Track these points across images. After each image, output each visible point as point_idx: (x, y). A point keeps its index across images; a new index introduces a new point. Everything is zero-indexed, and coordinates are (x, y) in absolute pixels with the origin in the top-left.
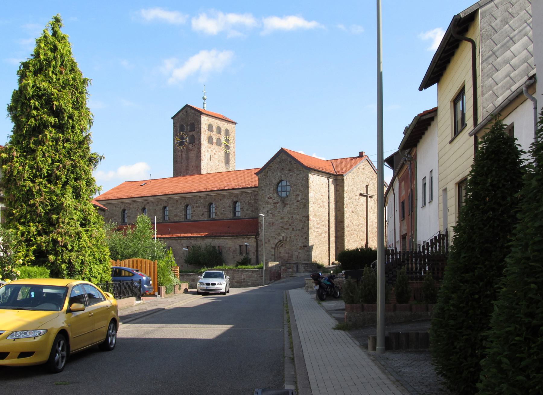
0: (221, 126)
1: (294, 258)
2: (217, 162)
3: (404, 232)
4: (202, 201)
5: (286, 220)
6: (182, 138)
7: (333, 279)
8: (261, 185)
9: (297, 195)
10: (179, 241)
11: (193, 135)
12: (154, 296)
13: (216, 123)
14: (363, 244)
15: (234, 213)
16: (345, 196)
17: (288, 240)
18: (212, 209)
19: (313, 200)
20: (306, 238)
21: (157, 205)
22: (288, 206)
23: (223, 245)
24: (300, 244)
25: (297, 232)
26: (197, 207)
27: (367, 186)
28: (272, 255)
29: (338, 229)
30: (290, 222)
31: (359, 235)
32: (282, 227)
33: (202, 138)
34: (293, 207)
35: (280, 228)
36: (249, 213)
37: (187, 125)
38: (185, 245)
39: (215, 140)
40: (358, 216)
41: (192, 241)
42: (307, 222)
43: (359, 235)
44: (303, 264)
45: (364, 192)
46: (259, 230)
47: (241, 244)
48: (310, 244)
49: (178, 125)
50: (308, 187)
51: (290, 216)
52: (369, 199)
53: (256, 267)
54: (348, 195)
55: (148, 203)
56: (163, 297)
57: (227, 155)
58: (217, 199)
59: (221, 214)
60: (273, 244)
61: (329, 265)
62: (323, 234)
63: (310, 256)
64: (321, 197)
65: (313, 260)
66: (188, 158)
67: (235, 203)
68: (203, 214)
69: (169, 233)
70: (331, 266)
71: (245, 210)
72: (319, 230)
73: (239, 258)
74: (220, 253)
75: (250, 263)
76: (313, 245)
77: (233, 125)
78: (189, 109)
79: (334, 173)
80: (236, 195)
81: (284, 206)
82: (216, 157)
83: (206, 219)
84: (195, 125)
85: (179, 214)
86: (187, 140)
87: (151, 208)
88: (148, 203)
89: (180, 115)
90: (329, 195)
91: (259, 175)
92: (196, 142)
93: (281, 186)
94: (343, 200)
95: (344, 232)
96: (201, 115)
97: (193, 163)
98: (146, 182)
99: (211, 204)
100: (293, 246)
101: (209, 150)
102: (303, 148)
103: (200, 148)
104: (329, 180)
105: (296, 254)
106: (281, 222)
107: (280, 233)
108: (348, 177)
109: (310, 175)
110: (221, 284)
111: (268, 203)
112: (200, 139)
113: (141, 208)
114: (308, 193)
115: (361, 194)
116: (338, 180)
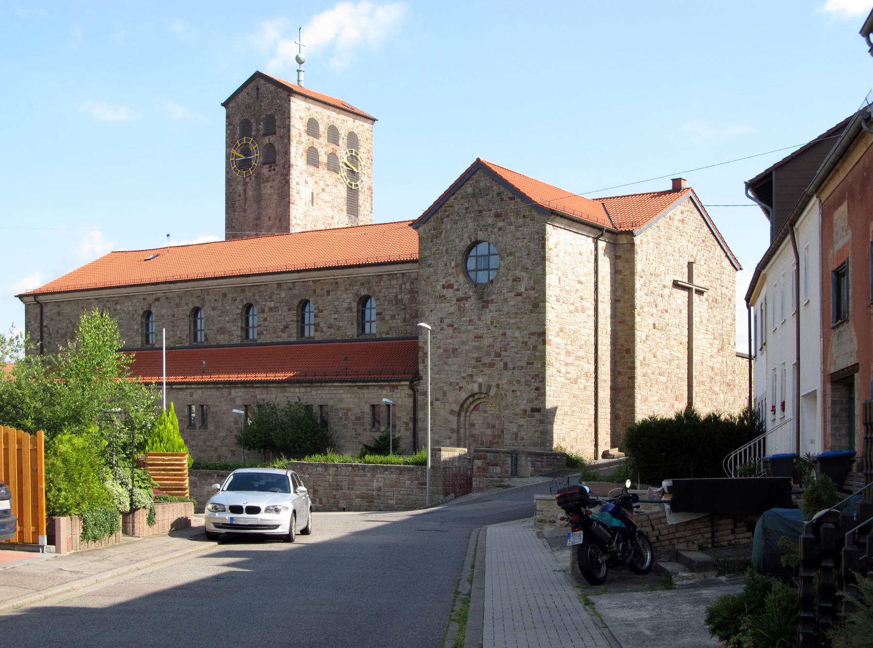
0: (338, 124)
1: (508, 439)
2: (329, 210)
3: (842, 362)
4: (283, 294)
5: (486, 341)
6: (246, 152)
7: (631, 509)
8: (427, 254)
9: (516, 280)
10: (225, 391)
11: (271, 146)
12: (35, 547)
13: (326, 117)
14: (681, 406)
15: (361, 325)
16: (638, 285)
17: (492, 393)
18: (307, 315)
19: (558, 292)
20: (537, 389)
21: (178, 306)
22: (492, 307)
23: (331, 403)
25: (516, 372)
26: (271, 309)
27: (690, 265)
28: (452, 431)
29: (619, 369)
30: (497, 346)
31: (670, 386)
32: (478, 360)
34: (505, 309)
35: (473, 362)
36: (397, 325)
37: (258, 118)
38: (239, 402)
39: (323, 159)
40: (668, 339)
41: (257, 391)
42: (540, 347)
43: (670, 386)
44: (531, 454)
45: (683, 279)
46: (421, 367)
47: (375, 402)
48: (549, 405)
49: (237, 121)
50: (544, 258)
51: (497, 332)
52: (695, 297)
53: (409, 459)
55: (157, 300)
56: (64, 552)
57: (353, 195)
58: (318, 291)
59: (330, 327)
60: (455, 402)
61: (596, 458)
62: (582, 381)
63: (547, 435)
64: (578, 286)
65: (555, 446)
66: (259, 199)
67: (363, 301)
68: (286, 327)
69: (204, 373)
70: (601, 460)
71: (388, 318)
72: (570, 369)
73: (370, 436)
74: (325, 423)
75: (397, 450)
76: (555, 409)
77: (367, 125)
78: (262, 81)
79: (608, 225)
81: (483, 307)
82: (325, 196)
84: (275, 121)
85: (229, 325)
86: (257, 156)
87: (163, 311)
88: (157, 300)
89: (241, 96)
90: (596, 283)
91: (421, 229)
92: (277, 160)
93: (477, 256)
94: (633, 297)
95: (633, 378)
96: (289, 96)
97: (271, 211)
98: (157, 253)
99: (305, 303)
100: (506, 407)
102: (534, 164)
104: (596, 244)
105: (513, 428)
106: (477, 348)
107: (471, 376)
108: (645, 239)
109: (549, 228)
110: (277, 511)
111: (442, 297)
112: (287, 153)
113: (141, 312)
114: (544, 274)
115: (676, 284)
116: (620, 244)
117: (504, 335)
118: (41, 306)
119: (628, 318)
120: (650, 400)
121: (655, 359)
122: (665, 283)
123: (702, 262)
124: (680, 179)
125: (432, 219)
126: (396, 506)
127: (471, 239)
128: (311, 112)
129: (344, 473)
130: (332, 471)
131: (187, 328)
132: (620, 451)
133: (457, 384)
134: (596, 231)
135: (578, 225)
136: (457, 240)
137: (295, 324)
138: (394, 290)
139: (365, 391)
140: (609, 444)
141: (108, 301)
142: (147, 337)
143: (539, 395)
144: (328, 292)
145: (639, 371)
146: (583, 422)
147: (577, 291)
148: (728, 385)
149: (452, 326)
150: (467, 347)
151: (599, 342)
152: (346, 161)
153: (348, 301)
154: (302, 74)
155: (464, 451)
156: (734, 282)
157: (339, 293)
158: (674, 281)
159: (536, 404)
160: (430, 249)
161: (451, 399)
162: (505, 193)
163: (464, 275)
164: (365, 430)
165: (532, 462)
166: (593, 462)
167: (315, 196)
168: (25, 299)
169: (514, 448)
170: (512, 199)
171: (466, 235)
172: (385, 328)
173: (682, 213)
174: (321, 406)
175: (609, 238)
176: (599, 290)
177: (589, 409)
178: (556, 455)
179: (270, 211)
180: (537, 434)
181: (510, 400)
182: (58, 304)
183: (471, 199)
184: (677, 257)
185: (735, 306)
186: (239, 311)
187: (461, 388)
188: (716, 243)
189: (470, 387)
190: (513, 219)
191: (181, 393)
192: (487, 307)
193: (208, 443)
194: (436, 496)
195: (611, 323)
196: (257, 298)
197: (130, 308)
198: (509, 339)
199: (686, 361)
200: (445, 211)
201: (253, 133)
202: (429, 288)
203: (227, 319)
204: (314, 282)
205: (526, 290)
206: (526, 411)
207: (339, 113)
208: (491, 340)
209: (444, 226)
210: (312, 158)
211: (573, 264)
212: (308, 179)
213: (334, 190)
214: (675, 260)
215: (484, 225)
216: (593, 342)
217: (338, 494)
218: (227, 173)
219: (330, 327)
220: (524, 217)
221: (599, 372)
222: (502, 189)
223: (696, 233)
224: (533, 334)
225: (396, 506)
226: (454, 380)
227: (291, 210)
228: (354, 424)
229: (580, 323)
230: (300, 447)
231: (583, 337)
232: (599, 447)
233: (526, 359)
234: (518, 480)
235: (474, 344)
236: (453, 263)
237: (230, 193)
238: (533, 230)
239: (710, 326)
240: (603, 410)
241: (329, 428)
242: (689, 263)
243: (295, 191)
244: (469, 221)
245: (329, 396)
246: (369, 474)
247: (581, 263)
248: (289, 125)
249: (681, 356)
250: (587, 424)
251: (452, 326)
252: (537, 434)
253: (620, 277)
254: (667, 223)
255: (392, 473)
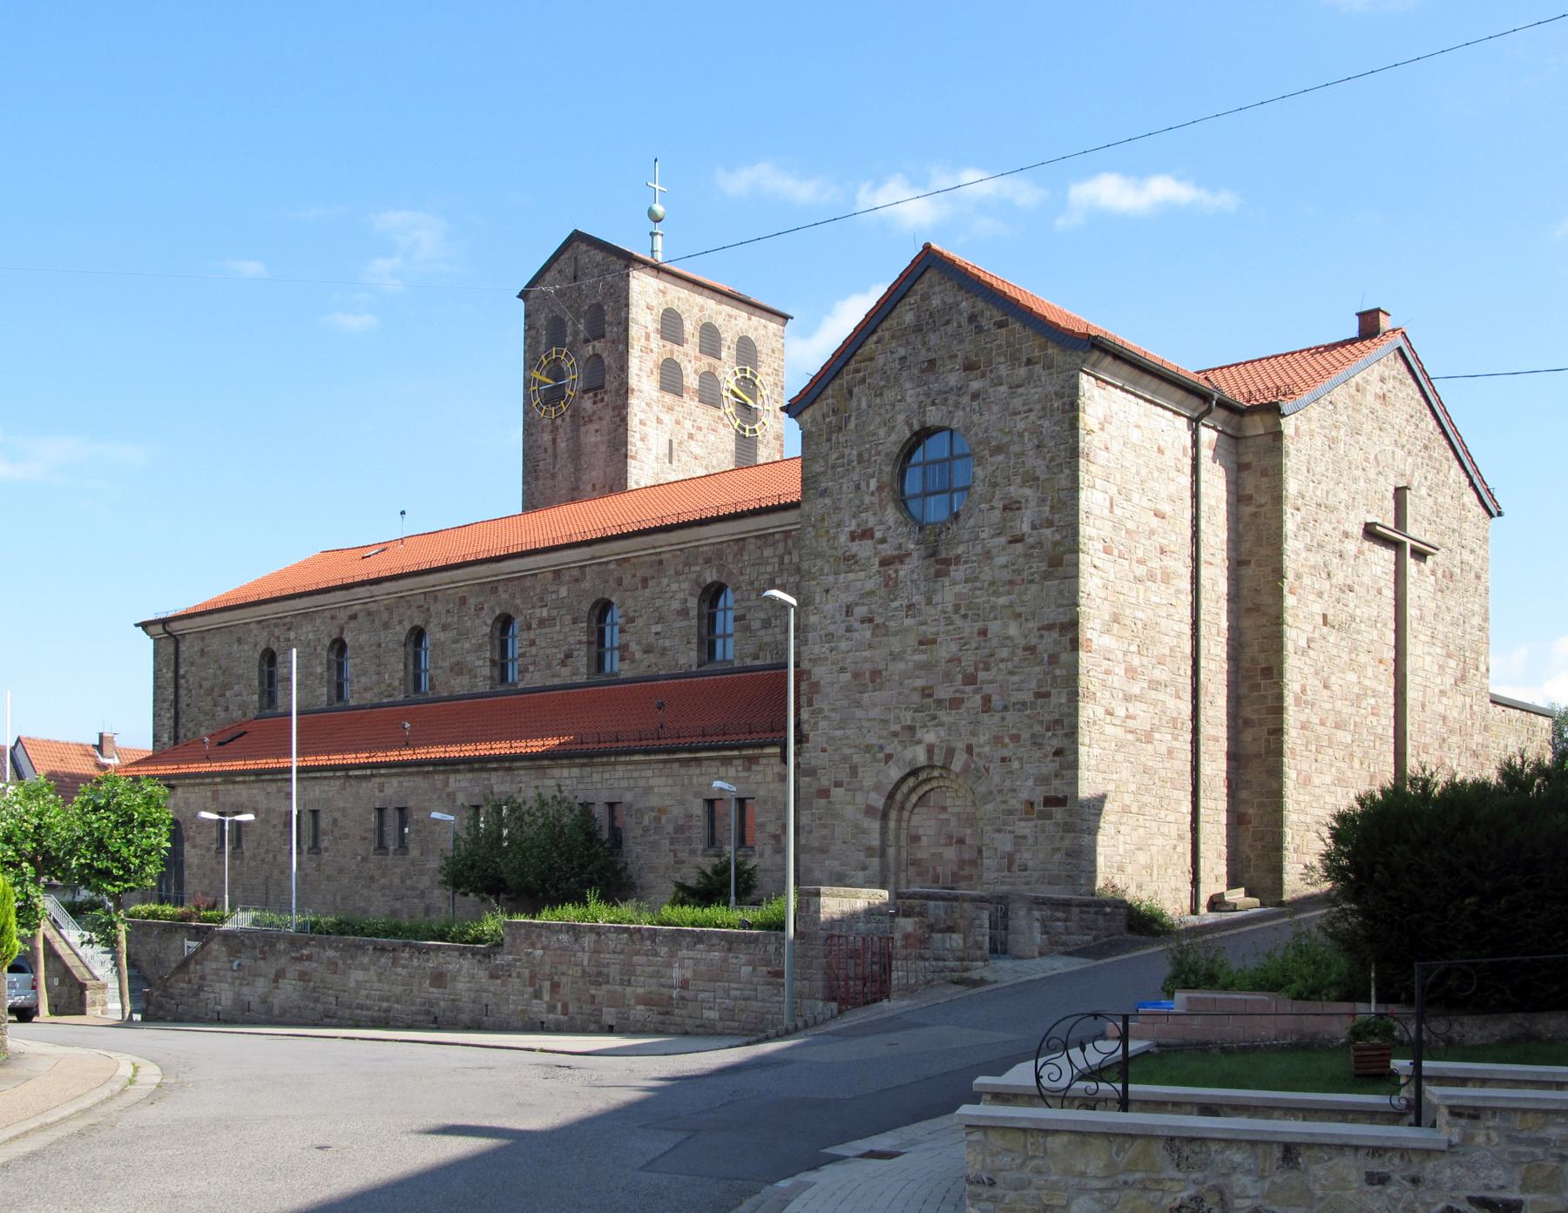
0: (719, 321)
4: (563, 592)
5: (945, 650)
6: (557, 373)
8: (817, 468)
9: (1012, 507)
11: (597, 357)
13: (696, 309)
15: (708, 645)
16: (1290, 526)
17: (957, 765)
19: (1107, 530)
20: (1058, 753)
22: (959, 572)
23: (628, 797)
24: (1030, 790)
25: (1011, 716)
26: (542, 623)
27: (1400, 494)
28: (870, 851)
29: (1248, 712)
30: (968, 660)
31: (1358, 752)
32: (926, 692)
33: (634, 363)
34: (987, 575)
35: (916, 697)
37: (576, 316)
39: (691, 381)
40: (1354, 649)
41: (494, 778)
42: (1064, 657)
43: (1358, 752)
44: (1039, 902)
48: (1086, 790)
49: (542, 321)
50: (1074, 453)
51: (969, 628)
54: (1303, 526)
55: (353, 617)
58: (627, 580)
59: (648, 650)
60: (877, 788)
62: (1164, 737)
63: (1082, 859)
65: (1100, 883)
66: (576, 454)
68: (568, 656)
70: (1207, 917)
71: (756, 625)
72: (1137, 708)
73: (697, 865)
76: (1101, 799)
77: (774, 326)
78: (584, 247)
80: (715, 556)
81: (938, 574)
82: (694, 447)
83: (582, 678)
84: (603, 314)
86: (574, 380)
87: (363, 638)
88: (353, 617)
91: (806, 415)
92: (607, 385)
95: (1278, 731)
96: (627, 267)
100: (988, 797)
101: (666, 417)
103: (625, 406)
105: (1004, 843)
106: (923, 666)
107: (911, 729)
108: (1304, 427)
109: (1086, 382)
111: (850, 560)
112: (624, 368)
113: (327, 642)
114: (1074, 488)
116: (1244, 428)
117: (983, 633)
118: (176, 640)
119: (1265, 599)
120: (1316, 781)
121: (1326, 693)
122: (1347, 527)
123: (1423, 491)
124: (1378, 310)
125: (829, 391)
126: (719, 1026)
127: (910, 426)
128: (668, 298)
129: (612, 945)
130: (588, 940)
131: (401, 666)
132: (1249, 894)
133: (881, 748)
134: (1196, 401)
135: (1155, 383)
136: (882, 432)
137: (584, 648)
138: (769, 568)
139: (694, 770)
140: (1224, 880)
141: (276, 625)
142: (340, 687)
143: (1062, 768)
144: (645, 581)
145: (1293, 716)
146: (1165, 829)
147: (1152, 532)
148: (1475, 754)
149: (871, 620)
150: (901, 666)
151: (1203, 652)
152: (733, 386)
153: (681, 595)
154: (658, 239)
155: (881, 896)
156: (1486, 540)
157: (665, 581)
158: (1367, 525)
159: (1057, 788)
160: (826, 457)
161: (868, 783)
162: (987, 314)
163: (898, 508)
164: (693, 852)
165: (1043, 921)
166: (1193, 920)
167: (675, 446)
168: (152, 629)
169: (1005, 888)
170: (1000, 325)
171: (901, 418)
172: (750, 649)
173: (1382, 380)
174: (611, 805)
175: (1224, 423)
176: (1203, 536)
177: (1178, 801)
178: (1105, 903)
179: (594, 474)
180: (1058, 857)
181: (997, 779)
182: (202, 634)
183: (912, 338)
184: (1372, 473)
185: (1487, 589)
186: (487, 630)
187: (889, 757)
188: (1451, 454)
189: (908, 754)
190: (1003, 370)
191: (364, 784)
192: (947, 574)
193: (408, 882)
194: (807, 1002)
195: (1229, 611)
196: (518, 602)
197: (311, 636)
198: (995, 642)
199: (1391, 700)
200: (857, 371)
201: (568, 340)
202: (823, 542)
203: (467, 646)
204: (619, 562)
205: (1034, 527)
206: (1032, 804)
207: (720, 303)
208: (954, 647)
209: (854, 403)
210: (670, 379)
211: (1143, 472)
212: (662, 416)
213: (712, 437)
214: (1367, 481)
215: (940, 392)
216: (1188, 650)
217: (601, 992)
218: (526, 413)
219: (648, 650)
220: (1029, 362)
221: (1202, 718)
222: (980, 305)
223: (1410, 428)
224: (1049, 627)
225: (719, 1026)
226: (875, 741)
227: (630, 469)
228: (672, 841)
229: (1158, 605)
230: (557, 890)
231: (1167, 639)
232: (1202, 886)
233: (1033, 685)
234: (1007, 964)
235: (917, 657)
236: (873, 484)
237: (531, 448)
238: (1049, 389)
239: (1440, 628)
240: (1212, 804)
241: (625, 849)
242: (1397, 489)
243: (637, 436)
244: (908, 385)
245: (624, 784)
246: (663, 950)
247: (1161, 471)
248: (627, 319)
249: (1381, 688)
250: (1174, 834)
251: (871, 620)
252: (1058, 857)
253: (1248, 510)
254: (1351, 397)
255: (711, 948)
